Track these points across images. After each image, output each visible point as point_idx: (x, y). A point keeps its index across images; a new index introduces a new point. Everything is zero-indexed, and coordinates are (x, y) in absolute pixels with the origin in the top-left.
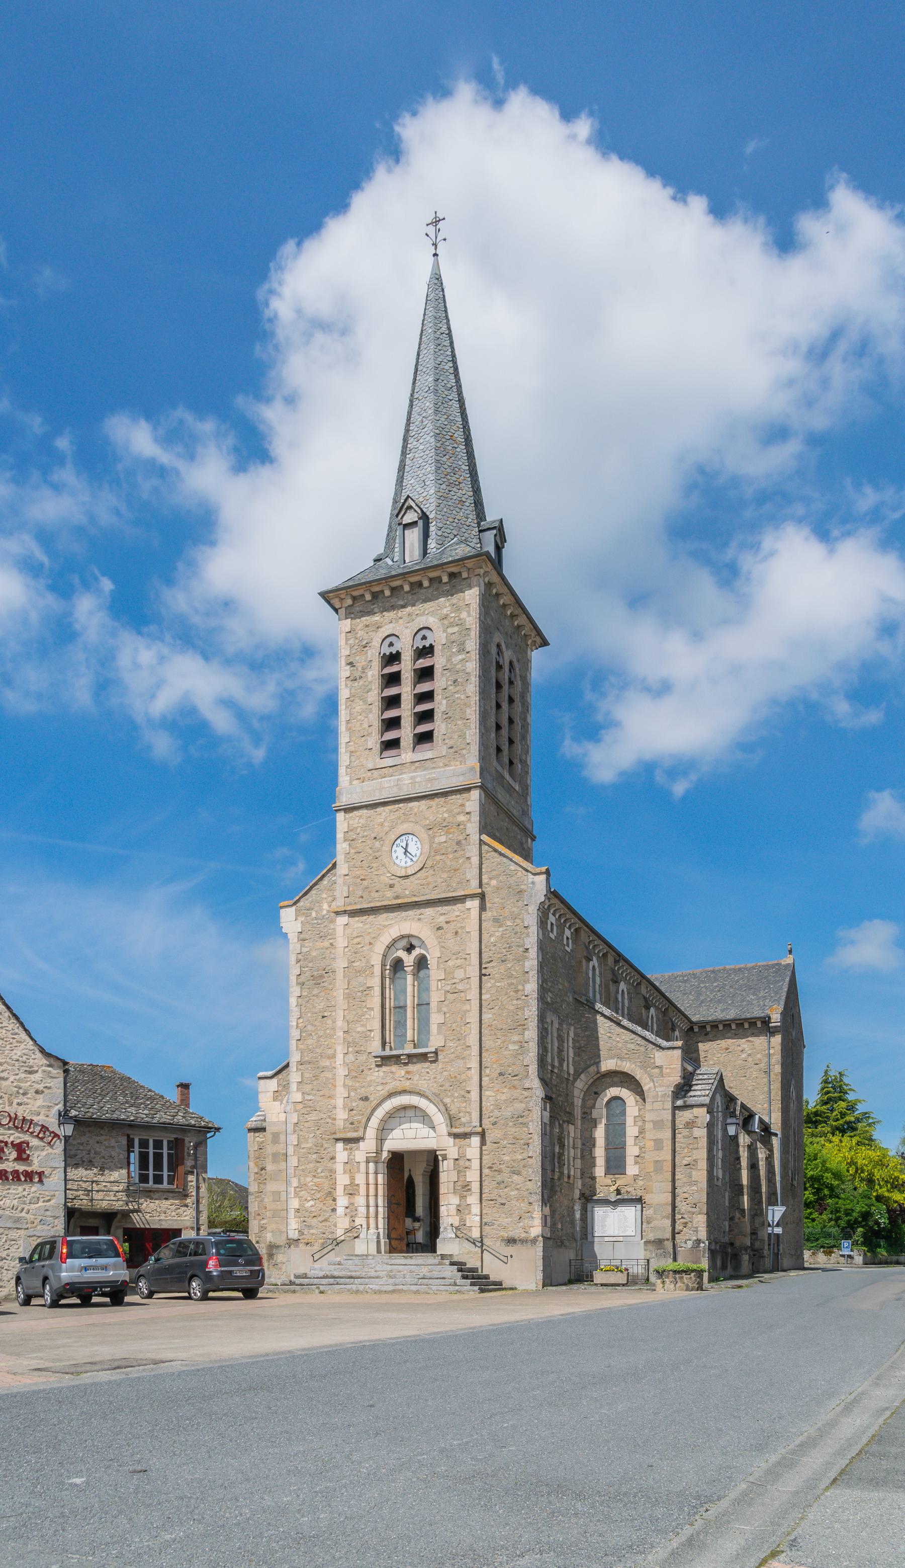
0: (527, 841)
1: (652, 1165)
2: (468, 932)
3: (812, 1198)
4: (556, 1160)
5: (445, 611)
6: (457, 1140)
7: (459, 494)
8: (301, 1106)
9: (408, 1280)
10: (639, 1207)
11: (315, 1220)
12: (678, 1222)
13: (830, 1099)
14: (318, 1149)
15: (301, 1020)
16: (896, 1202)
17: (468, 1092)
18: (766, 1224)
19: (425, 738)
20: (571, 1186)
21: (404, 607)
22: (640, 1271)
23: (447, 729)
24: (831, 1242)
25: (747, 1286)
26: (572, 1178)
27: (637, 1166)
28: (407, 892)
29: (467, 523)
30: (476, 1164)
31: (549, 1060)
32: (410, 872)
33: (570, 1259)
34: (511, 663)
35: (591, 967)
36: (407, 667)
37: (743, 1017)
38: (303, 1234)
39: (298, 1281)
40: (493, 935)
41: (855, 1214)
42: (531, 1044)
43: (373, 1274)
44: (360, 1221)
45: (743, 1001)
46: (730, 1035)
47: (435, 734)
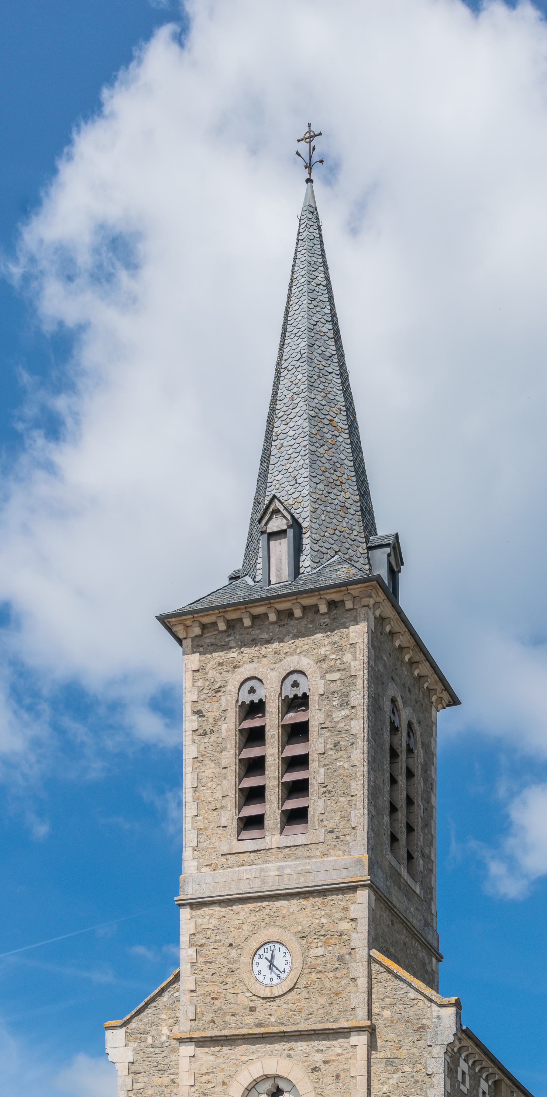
0: (431, 962)
5: (323, 651)
7: (340, 498)
19: (297, 817)
21: (269, 641)
23: (326, 807)
28: (273, 1019)
29: (352, 537)
34: (410, 725)
36: (272, 722)
47: (311, 812)
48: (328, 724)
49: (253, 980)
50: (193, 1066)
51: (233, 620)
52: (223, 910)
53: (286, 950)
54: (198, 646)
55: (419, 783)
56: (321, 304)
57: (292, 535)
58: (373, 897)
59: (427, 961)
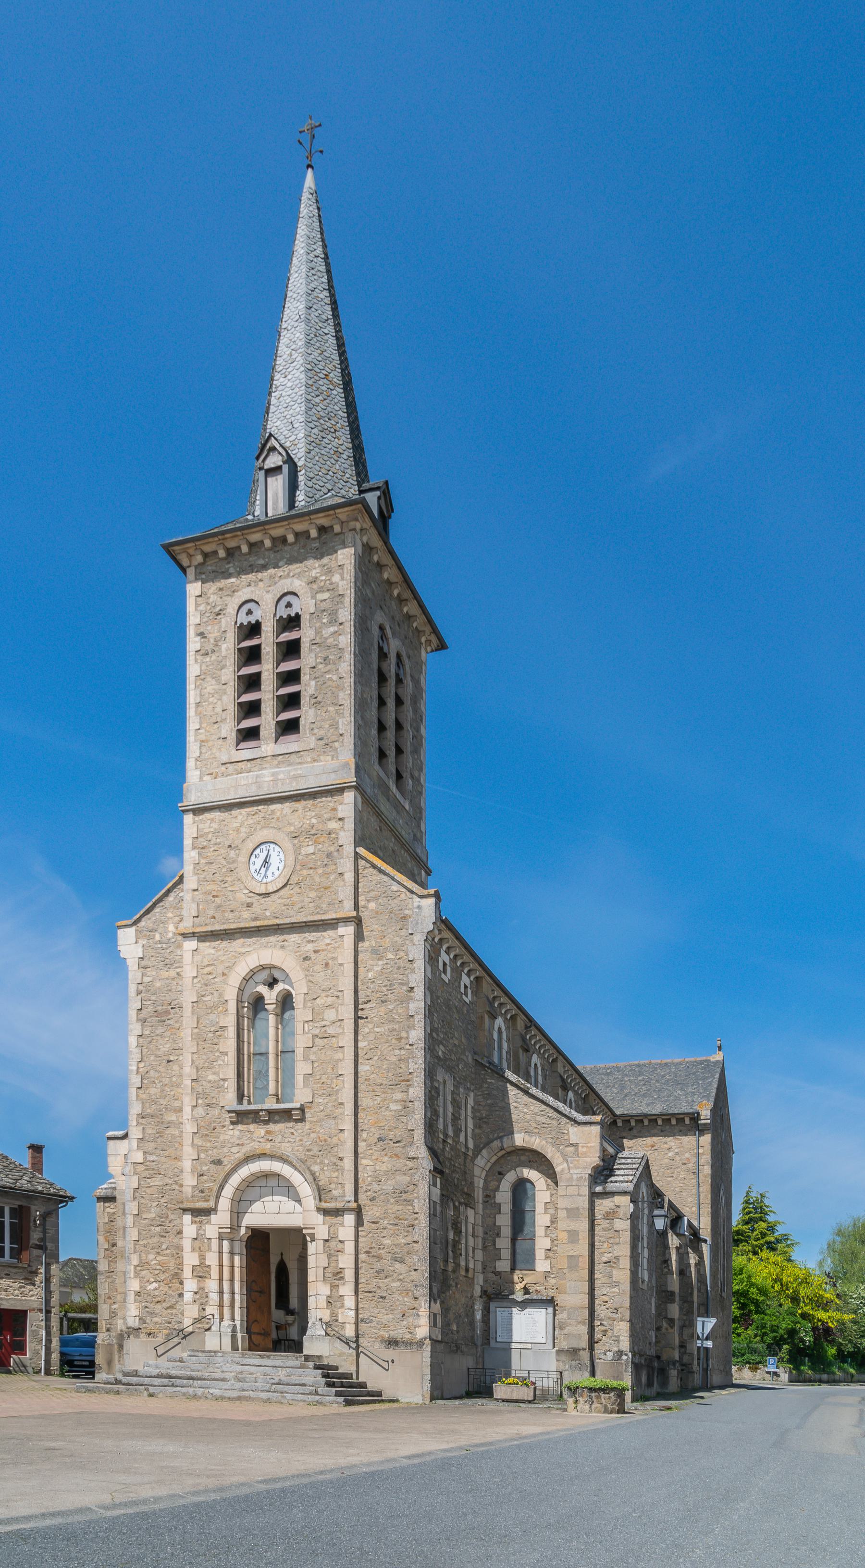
0: (420, 874)
1: (566, 1260)
2: (341, 964)
3: (737, 1313)
4: (450, 1248)
5: (314, 573)
6: (327, 1218)
7: (334, 444)
8: (142, 1167)
9: (259, 1385)
10: (550, 1310)
11: (159, 1306)
12: (597, 1329)
13: (751, 1219)
14: (162, 1221)
15: (142, 1065)
16: (819, 1320)
17: (341, 1159)
18: (695, 1336)
19: (290, 727)
20: (471, 1282)
21: (264, 567)
22: (551, 1385)
23: (316, 716)
24: (757, 1358)
25: (677, 1408)
26: (471, 1271)
27: (549, 1261)
28: (268, 914)
29: (345, 479)
30: (350, 1247)
31: (441, 1127)
32: (271, 889)
33: (469, 1366)
34: (399, 656)
35: (496, 1028)
36: (268, 641)
37: (670, 1112)
38: (145, 1322)
39: (125, 1379)
40: (371, 970)
41: (781, 1331)
42: (416, 1103)
43: (218, 1375)
44: (212, 1309)
45: (669, 1096)
46: (656, 1131)
47: (302, 722)
48: (318, 640)
49: (249, 878)
50: (195, 959)
51: (232, 548)
52: (223, 814)
53: (280, 850)
54: (200, 573)
55: (408, 711)
56: (319, 274)
57: (287, 469)
58: (360, 799)
59: (416, 871)
